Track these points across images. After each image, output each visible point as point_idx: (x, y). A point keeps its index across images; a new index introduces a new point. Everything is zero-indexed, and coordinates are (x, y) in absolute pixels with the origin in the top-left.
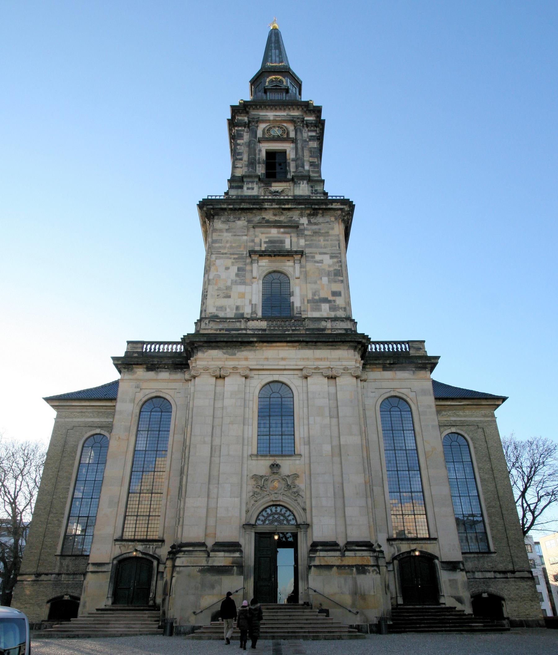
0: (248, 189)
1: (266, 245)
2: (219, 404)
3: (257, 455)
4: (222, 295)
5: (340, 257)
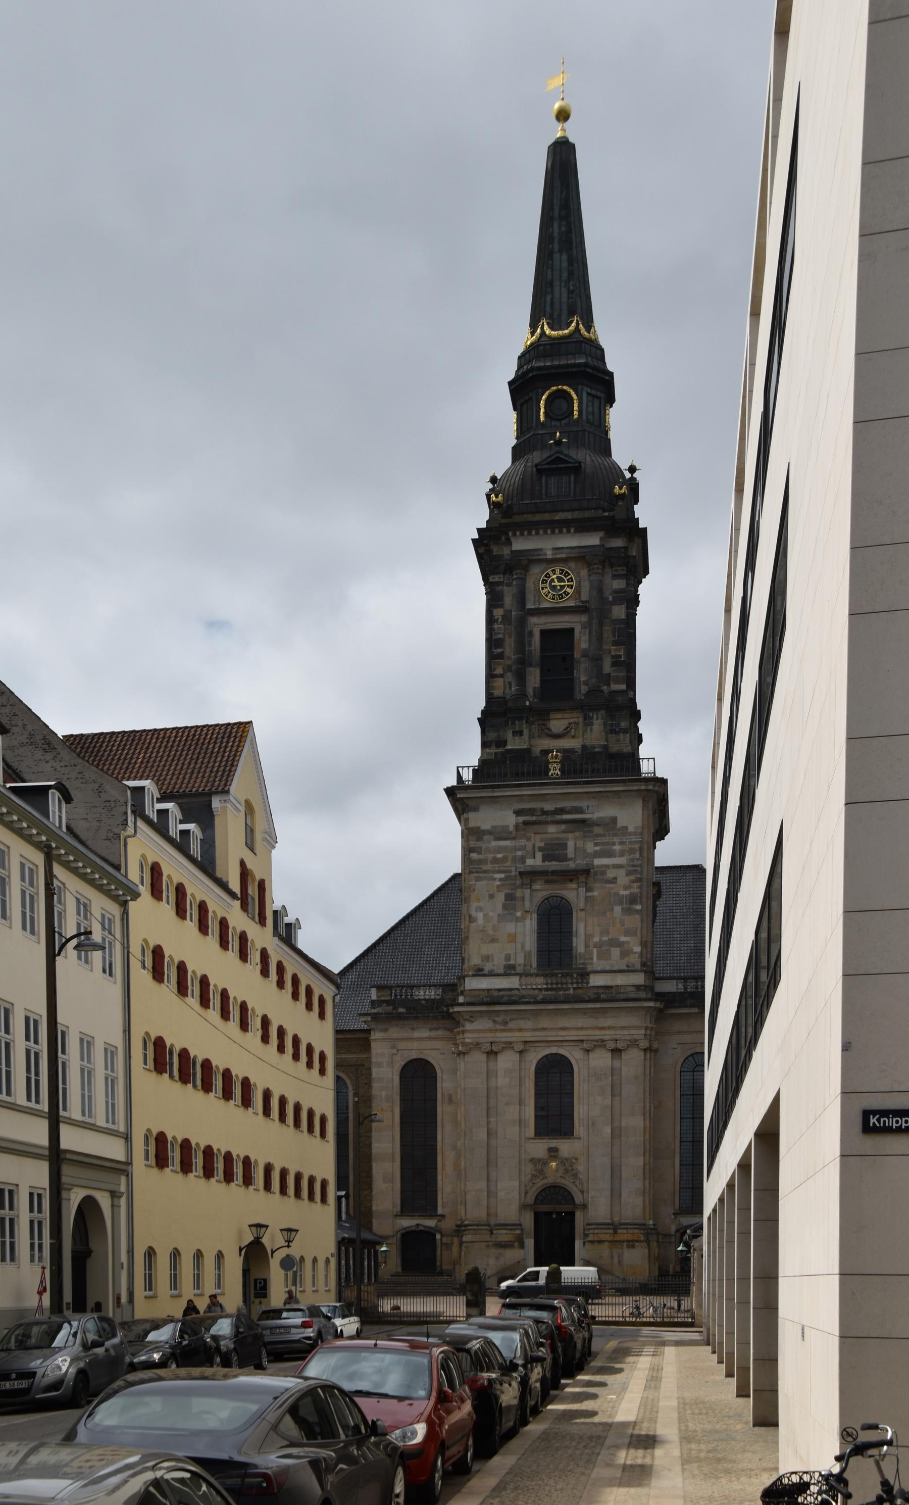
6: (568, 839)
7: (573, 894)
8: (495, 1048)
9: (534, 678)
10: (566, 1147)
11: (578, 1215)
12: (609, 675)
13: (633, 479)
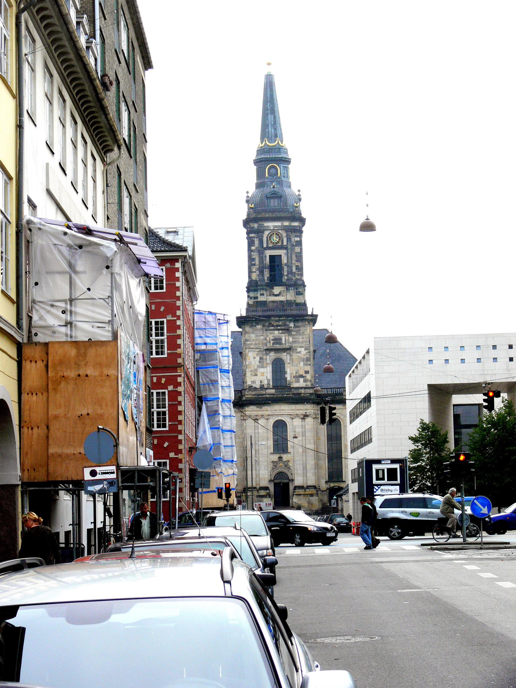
0: (261, 295)
1: (272, 342)
2: (257, 431)
3: (273, 453)
4: (253, 374)
5: (310, 349)
6: (282, 336)
7: (284, 356)
8: (257, 418)
9: (267, 274)
10: (285, 457)
11: (290, 484)
12: (295, 273)
13: (299, 195)
